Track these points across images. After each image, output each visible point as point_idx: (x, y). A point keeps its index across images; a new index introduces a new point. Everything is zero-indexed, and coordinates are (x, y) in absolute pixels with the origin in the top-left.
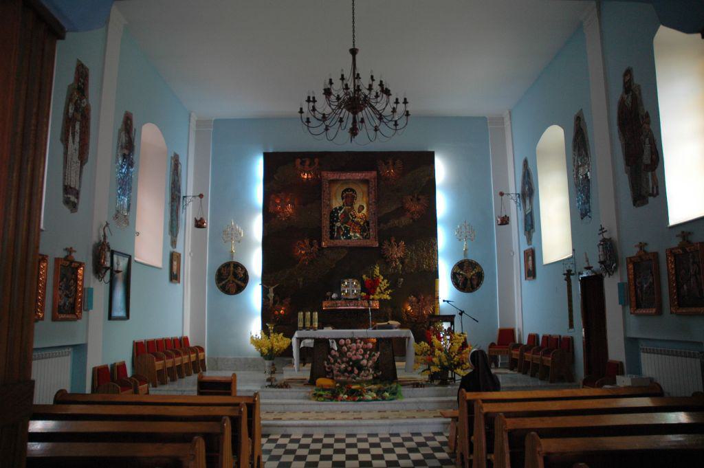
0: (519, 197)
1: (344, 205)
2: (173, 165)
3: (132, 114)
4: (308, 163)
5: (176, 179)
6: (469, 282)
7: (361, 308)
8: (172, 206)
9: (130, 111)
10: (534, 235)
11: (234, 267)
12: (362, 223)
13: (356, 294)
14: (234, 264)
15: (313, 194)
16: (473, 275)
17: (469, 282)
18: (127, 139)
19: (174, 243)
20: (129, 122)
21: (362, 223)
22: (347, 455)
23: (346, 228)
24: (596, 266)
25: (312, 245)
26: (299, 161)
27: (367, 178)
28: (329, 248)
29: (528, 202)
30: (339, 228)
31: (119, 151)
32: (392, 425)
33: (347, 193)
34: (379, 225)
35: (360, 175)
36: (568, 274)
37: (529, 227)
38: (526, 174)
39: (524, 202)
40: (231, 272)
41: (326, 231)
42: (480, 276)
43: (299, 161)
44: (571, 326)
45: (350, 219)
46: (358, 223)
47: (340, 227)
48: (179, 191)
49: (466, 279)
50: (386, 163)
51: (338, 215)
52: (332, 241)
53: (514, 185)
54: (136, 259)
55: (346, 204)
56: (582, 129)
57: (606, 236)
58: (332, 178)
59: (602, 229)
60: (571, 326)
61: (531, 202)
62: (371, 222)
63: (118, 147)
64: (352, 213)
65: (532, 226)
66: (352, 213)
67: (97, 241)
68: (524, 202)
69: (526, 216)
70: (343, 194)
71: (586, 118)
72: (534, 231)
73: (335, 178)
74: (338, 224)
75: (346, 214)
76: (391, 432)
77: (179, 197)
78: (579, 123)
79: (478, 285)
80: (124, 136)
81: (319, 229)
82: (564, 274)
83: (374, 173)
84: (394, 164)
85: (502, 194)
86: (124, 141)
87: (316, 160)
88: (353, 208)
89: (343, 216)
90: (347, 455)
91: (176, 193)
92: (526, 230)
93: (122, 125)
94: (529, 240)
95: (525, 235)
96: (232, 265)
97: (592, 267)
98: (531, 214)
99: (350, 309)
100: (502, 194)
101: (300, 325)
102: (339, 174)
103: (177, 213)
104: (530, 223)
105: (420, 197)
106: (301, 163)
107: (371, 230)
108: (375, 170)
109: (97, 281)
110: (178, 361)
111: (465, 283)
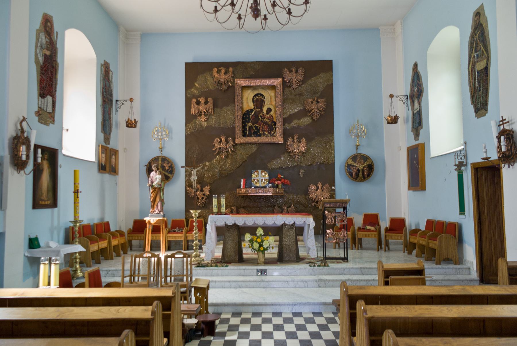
0: (407, 99)
1: (254, 108)
2: (103, 72)
3: (52, 17)
4: (223, 71)
5: (108, 84)
6: (361, 173)
7: (269, 194)
8: (104, 108)
9: (50, 13)
10: (422, 132)
11: (162, 161)
12: (270, 123)
13: (264, 183)
14: (162, 158)
15: (226, 95)
16: (365, 167)
17: (361, 173)
18: (48, 40)
19: (107, 140)
20: (49, 24)
21: (270, 123)
22: (248, 338)
23: (256, 127)
24: (494, 156)
25: (227, 142)
26: (215, 70)
27: (274, 84)
28: (241, 144)
29: (416, 102)
30: (250, 128)
31: (38, 51)
32: (295, 305)
33: (257, 97)
34: (284, 125)
35: (268, 81)
36: (460, 166)
37: (417, 125)
38: (416, 75)
39: (413, 103)
40: (160, 165)
41: (247, 140)
42: (371, 168)
43: (215, 70)
44: (462, 210)
45: (259, 119)
46: (266, 123)
47: (251, 126)
48: (111, 95)
49: (358, 170)
50: (291, 71)
51: (249, 117)
52: (244, 138)
53: (404, 87)
54: (64, 152)
55: (256, 106)
56: (481, 25)
57: (507, 127)
58: (244, 85)
59: (503, 120)
60: (462, 210)
61: (419, 103)
62: (277, 122)
63: (36, 47)
64: (261, 115)
65: (420, 123)
66: (261, 115)
67: (15, 135)
68: (413, 103)
69: (414, 115)
70: (253, 98)
71: (488, 13)
72: (422, 128)
73: (247, 84)
74: (250, 124)
75: (256, 115)
76: (294, 311)
77: (112, 101)
78: (479, 19)
79: (369, 175)
80: (43, 38)
81: (233, 128)
82: (455, 165)
83: (280, 80)
84: (297, 72)
85: (392, 96)
86: (44, 42)
87: (231, 69)
88: (262, 110)
89: (254, 117)
90: (248, 338)
91: (108, 96)
92: (413, 127)
93: (40, 26)
94: (417, 136)
95: (412, 131)
96: (160, 159)
97: (490, 158)
98: (419, 113)
99: (259, 196)
100: (392, 96)
101: (215, 210)
102: (250, 81)
103: (110, 114)
104: (418, 120)
105: (319, 100)
106: (217, 72)
107: (277, 129)
108: (280, 77)
109: (16, 172)
110: (103, 244)
111: (357, 174)
